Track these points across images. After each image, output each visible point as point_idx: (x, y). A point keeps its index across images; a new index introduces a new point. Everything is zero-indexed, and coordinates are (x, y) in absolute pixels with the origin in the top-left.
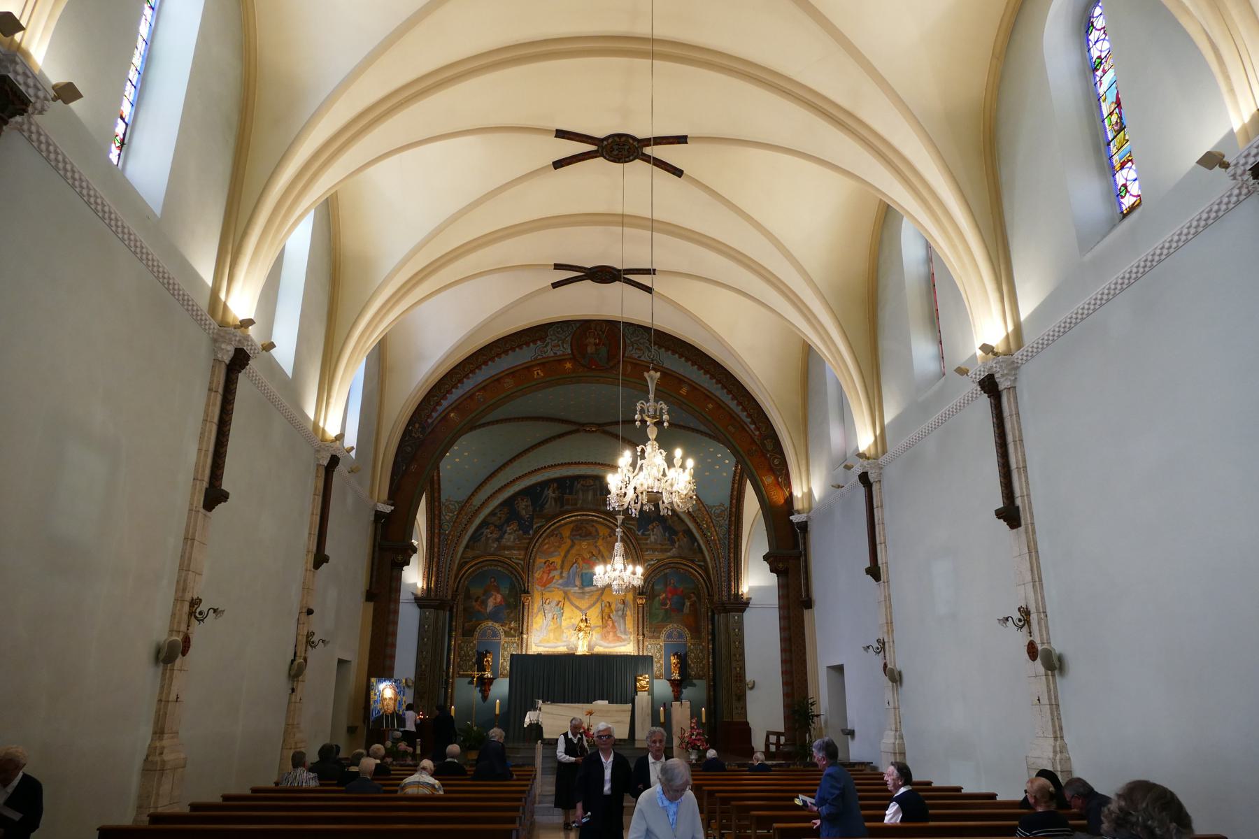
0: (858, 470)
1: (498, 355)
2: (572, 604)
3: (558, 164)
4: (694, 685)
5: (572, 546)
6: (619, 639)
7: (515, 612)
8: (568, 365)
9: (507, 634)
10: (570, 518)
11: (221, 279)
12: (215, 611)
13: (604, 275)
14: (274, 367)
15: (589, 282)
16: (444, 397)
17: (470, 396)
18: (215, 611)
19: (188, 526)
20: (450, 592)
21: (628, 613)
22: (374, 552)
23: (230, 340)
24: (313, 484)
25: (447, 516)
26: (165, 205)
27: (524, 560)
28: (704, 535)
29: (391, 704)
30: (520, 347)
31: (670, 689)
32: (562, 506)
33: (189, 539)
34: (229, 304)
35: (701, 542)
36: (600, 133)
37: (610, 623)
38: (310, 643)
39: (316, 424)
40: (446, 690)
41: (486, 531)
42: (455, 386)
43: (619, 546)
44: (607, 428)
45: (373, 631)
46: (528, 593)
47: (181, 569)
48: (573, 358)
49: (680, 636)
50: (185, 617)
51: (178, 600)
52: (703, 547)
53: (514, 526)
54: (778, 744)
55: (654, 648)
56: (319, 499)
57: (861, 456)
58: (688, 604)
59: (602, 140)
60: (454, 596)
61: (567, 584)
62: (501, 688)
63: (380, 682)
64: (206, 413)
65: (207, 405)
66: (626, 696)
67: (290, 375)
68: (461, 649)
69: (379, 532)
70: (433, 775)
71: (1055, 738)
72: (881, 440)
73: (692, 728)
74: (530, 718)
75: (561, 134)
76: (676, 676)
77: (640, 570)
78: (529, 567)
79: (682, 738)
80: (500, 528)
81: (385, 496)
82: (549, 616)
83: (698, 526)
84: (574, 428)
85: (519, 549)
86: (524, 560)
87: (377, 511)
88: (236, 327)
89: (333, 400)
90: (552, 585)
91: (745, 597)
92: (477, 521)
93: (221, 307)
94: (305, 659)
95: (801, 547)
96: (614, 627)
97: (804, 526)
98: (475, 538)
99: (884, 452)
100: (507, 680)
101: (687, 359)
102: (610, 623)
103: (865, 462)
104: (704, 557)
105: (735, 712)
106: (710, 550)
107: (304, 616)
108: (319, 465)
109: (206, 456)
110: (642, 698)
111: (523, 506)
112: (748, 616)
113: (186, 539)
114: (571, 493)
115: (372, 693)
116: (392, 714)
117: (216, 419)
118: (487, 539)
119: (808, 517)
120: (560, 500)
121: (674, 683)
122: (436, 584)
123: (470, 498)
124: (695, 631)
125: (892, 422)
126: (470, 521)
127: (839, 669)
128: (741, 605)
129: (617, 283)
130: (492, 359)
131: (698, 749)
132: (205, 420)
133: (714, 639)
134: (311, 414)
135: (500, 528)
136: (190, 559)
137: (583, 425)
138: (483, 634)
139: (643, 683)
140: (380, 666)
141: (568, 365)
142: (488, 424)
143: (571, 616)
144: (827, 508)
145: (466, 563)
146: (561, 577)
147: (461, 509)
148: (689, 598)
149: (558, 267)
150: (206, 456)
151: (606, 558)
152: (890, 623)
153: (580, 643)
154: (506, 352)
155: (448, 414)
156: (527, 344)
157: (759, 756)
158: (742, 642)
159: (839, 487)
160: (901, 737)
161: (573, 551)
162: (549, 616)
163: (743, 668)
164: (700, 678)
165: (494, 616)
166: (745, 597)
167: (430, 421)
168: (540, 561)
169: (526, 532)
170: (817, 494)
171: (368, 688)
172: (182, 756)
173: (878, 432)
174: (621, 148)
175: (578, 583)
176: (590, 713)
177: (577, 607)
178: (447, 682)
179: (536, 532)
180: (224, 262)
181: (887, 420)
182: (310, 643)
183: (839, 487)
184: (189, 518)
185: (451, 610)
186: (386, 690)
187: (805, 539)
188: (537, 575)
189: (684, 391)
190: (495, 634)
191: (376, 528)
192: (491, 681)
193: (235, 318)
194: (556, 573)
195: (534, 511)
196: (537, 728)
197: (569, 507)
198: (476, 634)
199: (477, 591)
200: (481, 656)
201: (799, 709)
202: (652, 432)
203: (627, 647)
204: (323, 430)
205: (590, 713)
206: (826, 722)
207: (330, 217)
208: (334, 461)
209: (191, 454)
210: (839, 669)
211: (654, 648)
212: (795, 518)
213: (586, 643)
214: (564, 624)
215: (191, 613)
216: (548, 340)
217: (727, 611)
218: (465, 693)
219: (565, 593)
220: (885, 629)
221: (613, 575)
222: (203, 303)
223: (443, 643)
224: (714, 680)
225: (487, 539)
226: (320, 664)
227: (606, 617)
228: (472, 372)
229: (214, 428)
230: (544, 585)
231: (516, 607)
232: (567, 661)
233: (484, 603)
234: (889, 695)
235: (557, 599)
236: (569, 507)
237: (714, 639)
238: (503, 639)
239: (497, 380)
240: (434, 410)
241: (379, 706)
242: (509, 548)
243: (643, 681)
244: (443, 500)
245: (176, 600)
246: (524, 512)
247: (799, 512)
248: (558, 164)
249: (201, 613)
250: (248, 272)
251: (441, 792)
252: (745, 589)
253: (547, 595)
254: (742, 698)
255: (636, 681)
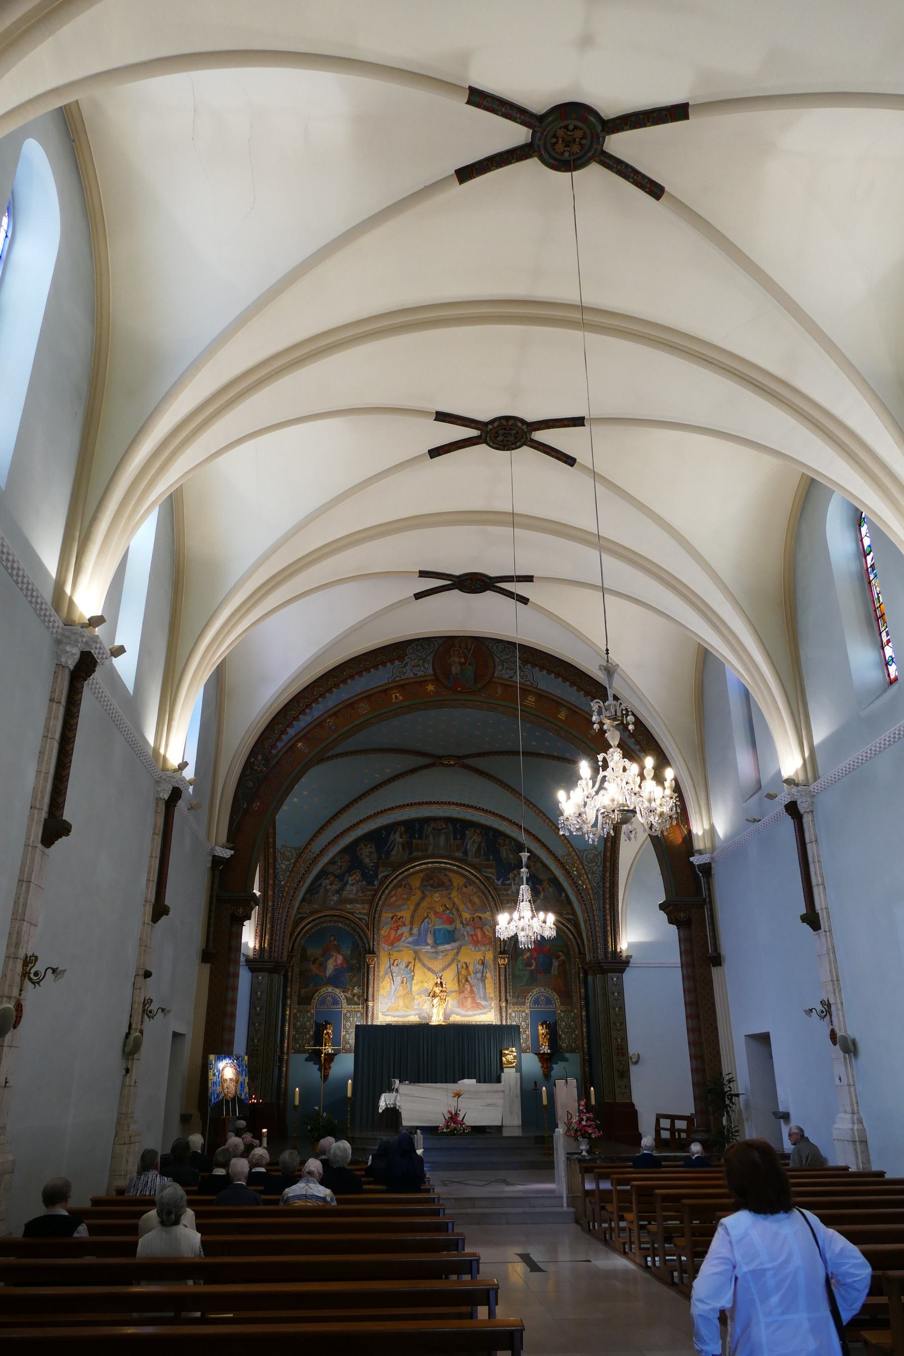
0: (784, 798)
1: (351, 677)
2: (424, 965)
3: (435, 453)
4: (566, 1060)
5: (422, 899)
6: (478, 1006)
7: (359, 976)
8: (430, 688)
9: (350, 1002)
10: (419, 866)
11: (67, 570)
12: (54, 971)
13: (474, 583)
14: (114, 677)
15: (456, 592)
16: (290, 725)
17: (320, 724)
18: (54, 971)
19: (23, 865)
20: (285, 953)
21: (488, 975)
22: (211, 904)
23: (76, 641)
24: (153, 820)
25: (282, 865)
26: (8, 483)
27: (368, 915)
28: (574, 884)
29: (232, 1086)
30: (376, 667)
31: (539, 1064)
32: (411, 853)
33: (24, 882)
34: (76, 599)
35: (570, 891)
36: (485, 416)
37: (467, 986)
38: (147, 1013)
39: (156, 751)
40: (280, 1068)
41: (325, 882)
42: (303, 712)
43: (525, 890)
44: (468, 762)
45: (210, 997)
46: (373, 953)
47: (14, 919)
48: (436, 680)
49: (548, 1001)
50: (18, 979)
51: (10, 957)
52: (573, 898)
53: (357, 876)
54: (672, 1130)
55: (518, 1016)
56: (159, 839)
57: (789, 782)
58: (556, 963)
59: (486, 424)
60: (290, 957)
61: (417, 942)
62: (345, 1065)
63: (219, 1059)
64: (47, 728)
65: (48, 719)
66: (491, 1074)
67: (131, 692)
68: (296, 1017)
69: (217, 880)
70: (323, 1182)
71: (853, 1113)
72: (811, 762)
73: (580, 1111)
74: (385, 1101)
75: (441, 417)
76: (545, 1049)
77: (551, 918)
78: (373, 923)
79: (569, 1124)
80: (341, 878)
81: (223, 838)
82: (398, 980)
83: (568, 873)
84: (428, 761)
85: (363, 902)
86: (368, 915)
87: (214, 856)
88: (83, 626)
89: (175, 723)
90: (400, 944)
91: (624, 955)
92: (316, 870)
93: (67, 599)
94: (141, 1032)
95: (705, 893)
96: (472, 991)
97: (707, 869)
98: (312, 890)
99: (816, 778)
100: (352, 1056)
101: (565, 680)
102: (467, 986)
103: (794, 789)
104: (573, 909)
105: (617, 1090)
106: (581, 900)
107: (141, 979)
108: (158, 799)
109: (46, 779)
110: (509, 1074)
111: (367, 854)
112: (629, 977)
113: (20, 881)
114: (420, 838)
115: (211, 1074)
116: (233, 1099)
117: (57, 736)
118: (326, 891)
119: (713, 859)
120: (408, 846)
121: (542, 1057)
122: (270, 944)
123: (309, 843)
124: (566, 996)
125: (824, 743)
126: (308, 870)
127: (763, 1039)
128: (620, 964)
129: (488, 593)
130: (344, 681)
131: (589, 1137)
132: (45, 737)
133: (587, 1005)
134: (151, 740)
135: (341, 878)
136: (25, 905)
137: (440, 757)
138: (323, 1002)
139: (510, 1058)
140: (217, 1043)
141: (430, 688)
142: (341, 755)
143: (423, 980)
144: (736, 847)
145: (303, 919)
146: (411, 934)
147: (299, 856)
148: (558, 957)
149: (423, 574)
150: (46, 779)
151: (512, 903)
152: (836, 981)
153: (435, 1010)
154: (360, 673)
155: (295, 744)
156: (384, 664)
157: (647, 1141)
158: (622, 1008)
159: (755, 821)
160: (860, 1121)
161: (424, 904)
162: (398, 980)
163: (625, 1039)
164: (573, 1051)
165: (336, 981)
166: (624, 955)
167: (274, 752)
168: (386, 916)
169: (370, 883)
170: (722, 829)
171: (205, 1067)
172: (10, 1158)
173: (807, 754)
174: (507, 433)
175: (430, 941)
176: (458, 1095)
177: (429, 969)
178: (281, 1060)
179: (381, 883)
180: (71, 550)
181: (817, 739)
182: (147, 1013)
183: (755, 821)
184: (25, 855)
185: (285, 976)
186: (226, 1070)
187: (709, 883)
188: (383, 932)
189: (562, 715)
190: (336, 1002)
191: (213, 876)
192: (330, 1058)
193: (81, 615)
194: (405, 930)
195: (379, 858)
196: (393, 1113)
197: (420, 854)
198: (314, 1001)
199: (314, 951)
200: (320, 1028)
201: (712, 1087)
202: (613, 737)
203: (488, 1016)
204: (164, 757)
205: (458, 1095)
206: (747, 1104)
207: (174, 512)
208: (176, 793)
209: (30, 776)
210: (763, 1039)
211: (518, 1016)
212: (696, 860)
213: (442, 1012)
214: (415, 988)
215: (25, 974)
216: (407, 660)
217: (604, 972)
218: (301, 1073)
219: (416, 952)
220: (830, 988)
221: (521, 923)
222: (47, 595)
223: (277, 1014)
224: (589, 1053)
225: (326, 891)
226: (156, 1036)
227: (463, 980)
228: (322, 695)
229: (56, 746)
230: (392, 944)
231: (359, 969)
232: (420, 1033)
233: (323, 966)
234: (839, 1069)
235: (406, 960)
236: (420, 854)
237: (587, 1005)
238: (345, 1008)
239: (351, 705)
240: (279, 739)
241: (219, 1089)
242: (351, 901)
243: (510, 1055)
244: (279, 845)
245: (8, 957)
246: (367, 860)
247: (700, 852)
248: (435, 453)
249: (36, 974)
250: (96, 563)
251: (334, 1203)
252: (623, 945)
253: (395, 955)
254: (625, 1074)
255: (501, 1055)
